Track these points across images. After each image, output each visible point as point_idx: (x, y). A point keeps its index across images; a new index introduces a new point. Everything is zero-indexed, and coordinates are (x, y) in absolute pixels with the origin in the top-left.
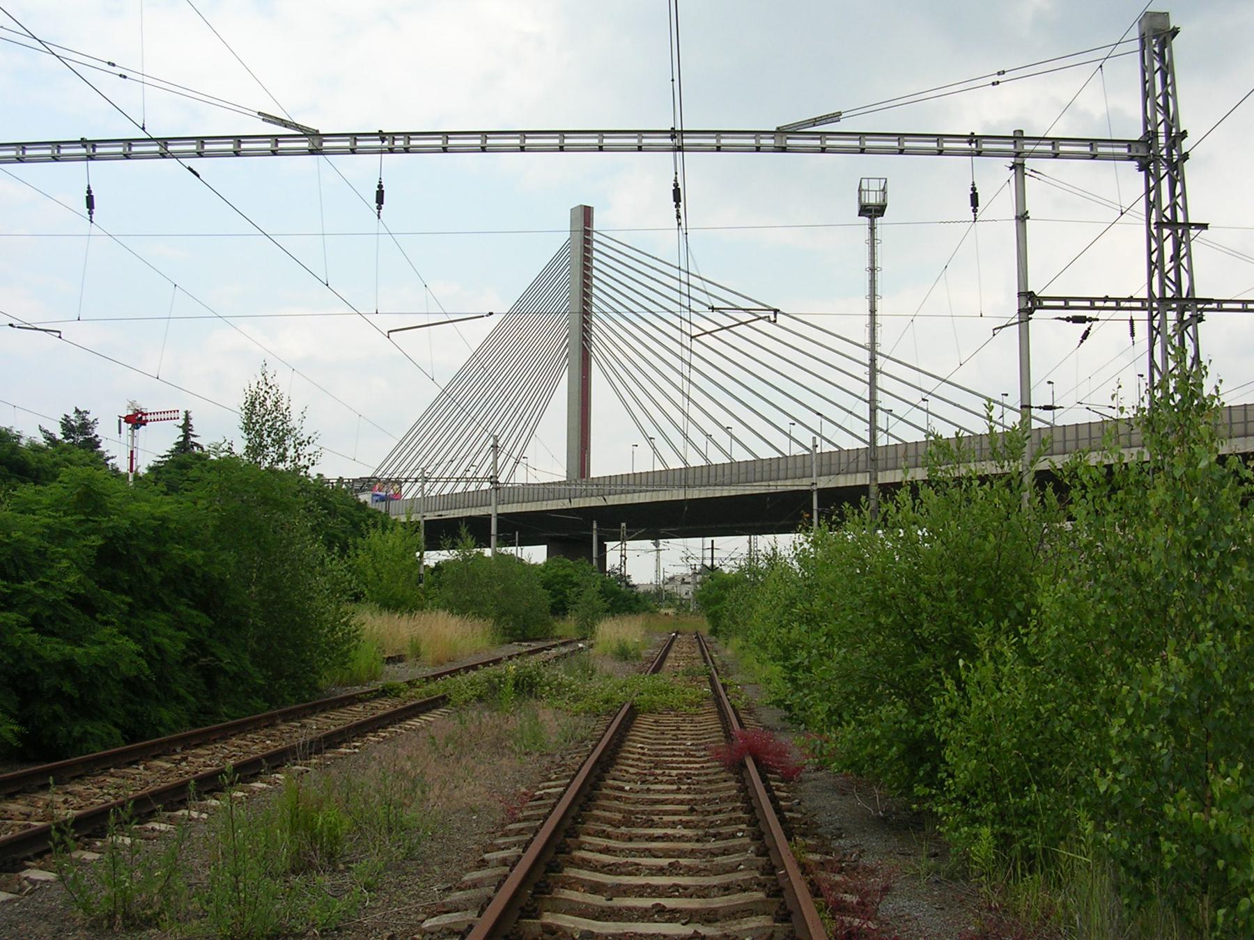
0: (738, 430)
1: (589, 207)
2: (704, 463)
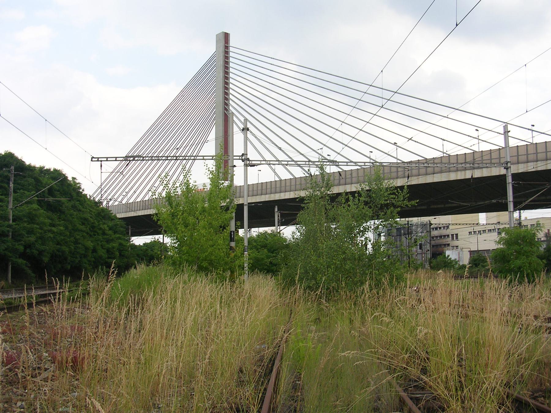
1: (228, 33)
2: (292, 177)
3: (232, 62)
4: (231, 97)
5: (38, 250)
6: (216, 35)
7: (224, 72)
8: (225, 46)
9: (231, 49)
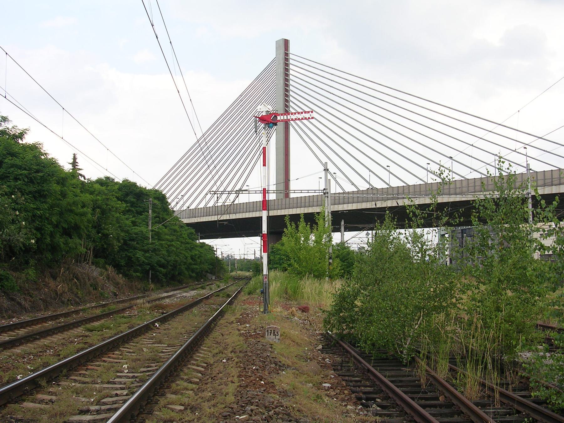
0: (394, 168)
2: (356, 190)
4: (291, 104)
9: (291, 56)
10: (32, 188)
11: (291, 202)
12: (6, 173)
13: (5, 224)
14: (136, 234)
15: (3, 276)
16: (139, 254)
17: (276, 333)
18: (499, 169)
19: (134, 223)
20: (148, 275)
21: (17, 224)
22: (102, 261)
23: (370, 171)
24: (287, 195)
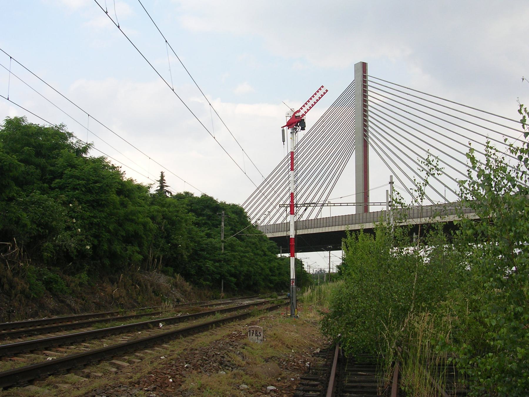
3: (370, 96)
4: (370, 123)
5: (239, 271)
6: (355, 65)
7: (362, 85)
8: (363, 80)
9: (369, 78)
10: (89, 197)
11: (368, 216)
12: (66, 183)
13: (59, 230)
14: (207, 244)
15: (52, 279)
16: (209, 264)
17: (258, 334)
18: (486, 155)
19: (209, 235)
20: (220, 284)
21: (73, 231)
22: (171, 270)
23: (446, 186)
24: (366, 209)
